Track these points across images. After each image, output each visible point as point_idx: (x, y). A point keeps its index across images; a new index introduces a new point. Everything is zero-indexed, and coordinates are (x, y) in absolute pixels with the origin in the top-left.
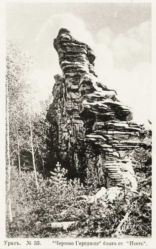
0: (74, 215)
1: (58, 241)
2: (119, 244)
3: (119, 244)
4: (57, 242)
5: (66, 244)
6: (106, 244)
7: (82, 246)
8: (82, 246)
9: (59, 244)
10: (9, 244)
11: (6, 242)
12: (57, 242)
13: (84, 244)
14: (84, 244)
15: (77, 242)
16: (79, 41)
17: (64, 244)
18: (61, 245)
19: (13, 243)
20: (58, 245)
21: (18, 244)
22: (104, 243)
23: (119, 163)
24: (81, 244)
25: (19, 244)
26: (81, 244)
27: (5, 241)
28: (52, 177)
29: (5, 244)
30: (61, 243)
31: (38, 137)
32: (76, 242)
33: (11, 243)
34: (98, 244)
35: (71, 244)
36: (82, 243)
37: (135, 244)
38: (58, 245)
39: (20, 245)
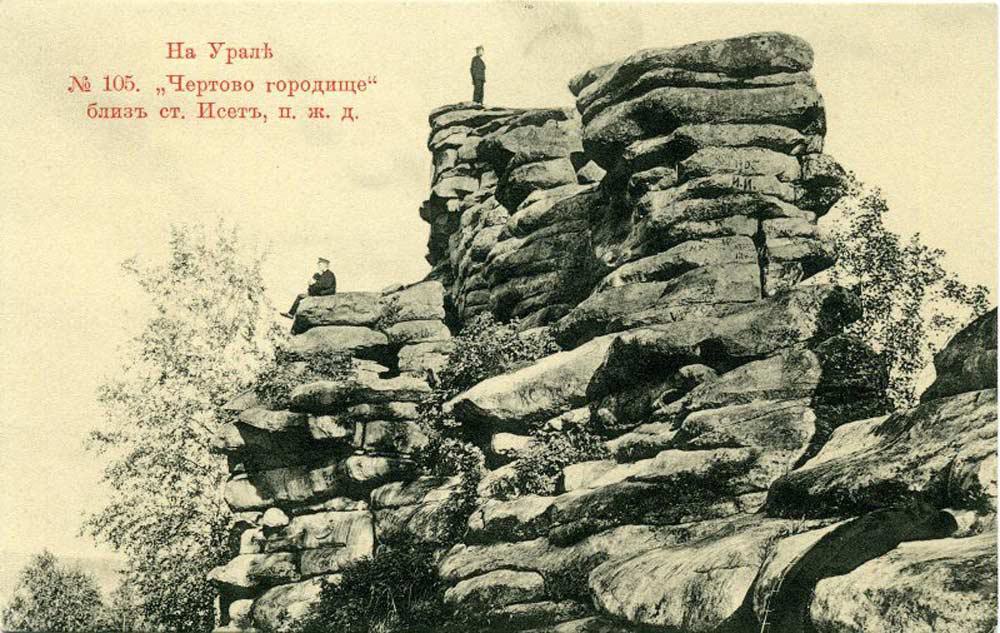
0: (743, 193)
1: (170, 57)
2: (165, 113)
3: (252, 85)
4: (175, 80)
5: (217, 87)
6: (99, 113)
7: (291, 95)
8: (291, 95)
9: (187, 85)
10: (229, 56)
11: (216, 46)
12: (175, 80)
13: (300, 86)
14: (300, 86)
15: (271, 86)
16: (242, 505)
17: (210, 87)
18: (197, 89)
19: (249, 52)
20: (180, 89)
21: (256, 114)
22: (92, 113)
23: (723, 562)
24: (285, 87)
25: (260, 115)
26: (285, 87)
27: (212, 44)
28: (377, 499)
29: (211, 50)
30: (197, 84)
31: (503, 211)
32: (269, 84)
33: (239, 53)
34: (362, 88)
35: (242, 85)
36: (291, 83)
37: (222, 113)
38: (180, 89)
39: (328, 116)
